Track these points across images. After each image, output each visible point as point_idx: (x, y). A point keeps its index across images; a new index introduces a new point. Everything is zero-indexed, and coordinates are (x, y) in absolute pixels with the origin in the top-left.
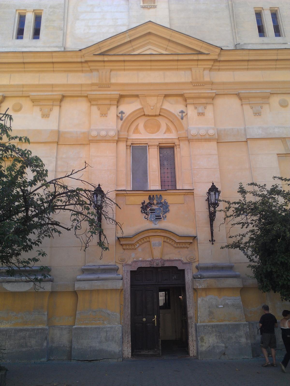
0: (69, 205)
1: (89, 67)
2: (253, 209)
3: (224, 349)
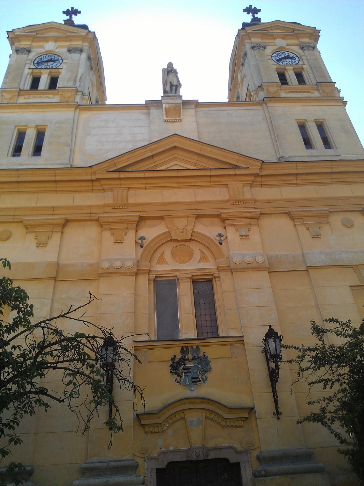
0: (64, 361)
1: (102, 186)
2: (340, 357)
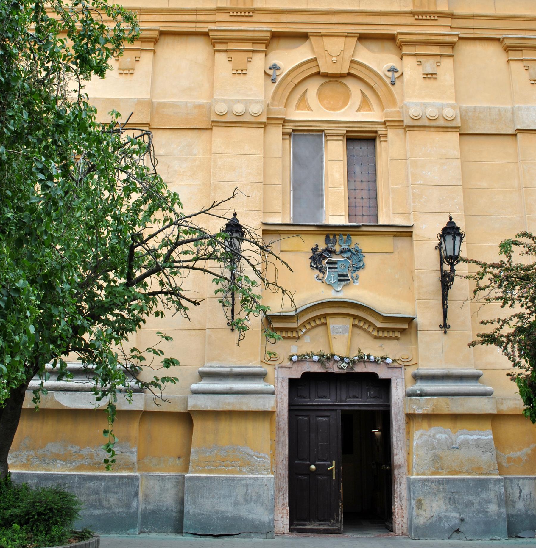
3: (457, 521)
